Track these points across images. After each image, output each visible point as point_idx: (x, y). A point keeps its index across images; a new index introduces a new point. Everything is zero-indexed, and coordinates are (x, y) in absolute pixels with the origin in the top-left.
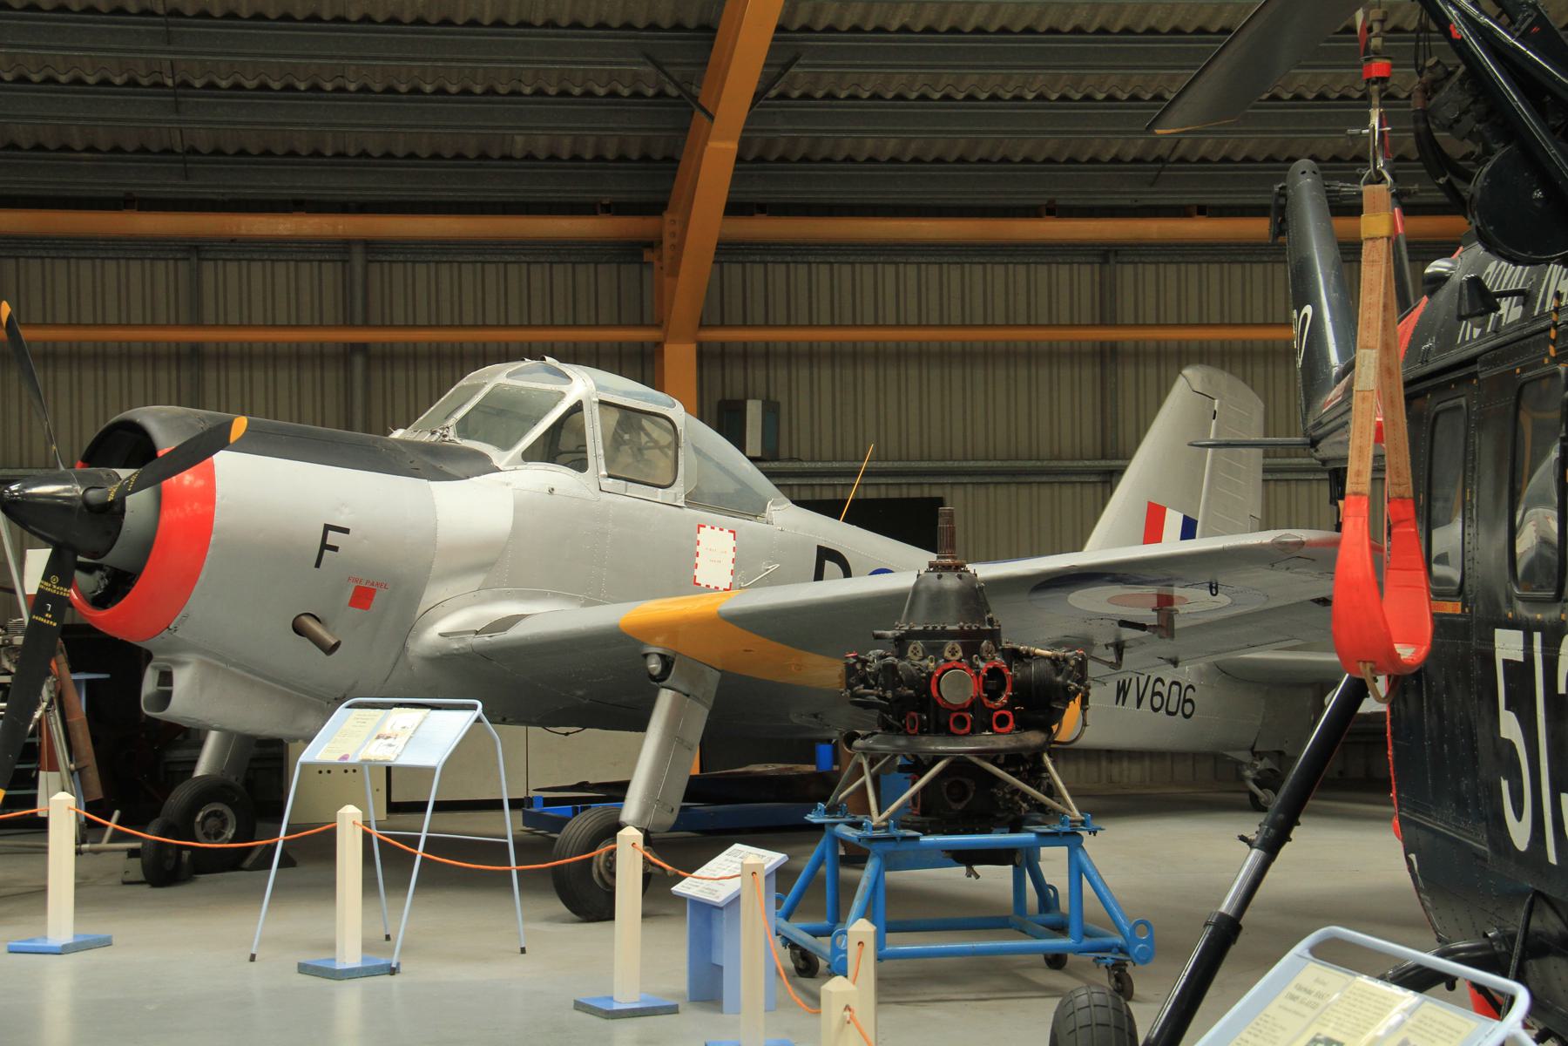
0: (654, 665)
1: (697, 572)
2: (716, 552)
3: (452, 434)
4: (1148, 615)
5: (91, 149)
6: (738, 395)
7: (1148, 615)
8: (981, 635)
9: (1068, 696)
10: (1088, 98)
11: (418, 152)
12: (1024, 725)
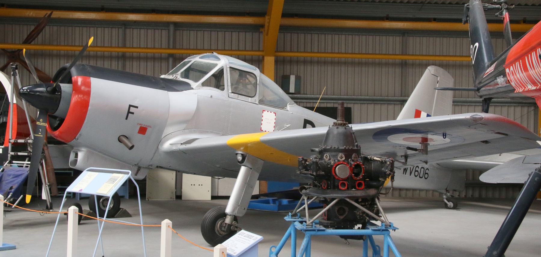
0: (240, 158)
1: (262, 126)
2: (269, 118)
4: (417, 145)
6: (288, 74)
7: (417, 145)
8: (353, 151)
9: (385, 176)
12: (369, 187)
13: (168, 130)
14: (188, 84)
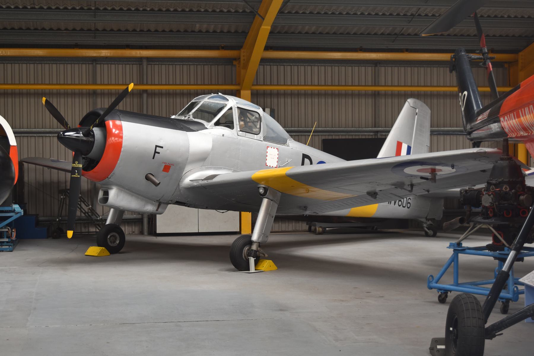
0: (261, 191)
1: (267, 162)
3: (191, 117)
5: (66, 29)
7: (427, 175)
10: (377, 14)
11: (166, 30)
13: (187, 168)
14: (202, 125)
